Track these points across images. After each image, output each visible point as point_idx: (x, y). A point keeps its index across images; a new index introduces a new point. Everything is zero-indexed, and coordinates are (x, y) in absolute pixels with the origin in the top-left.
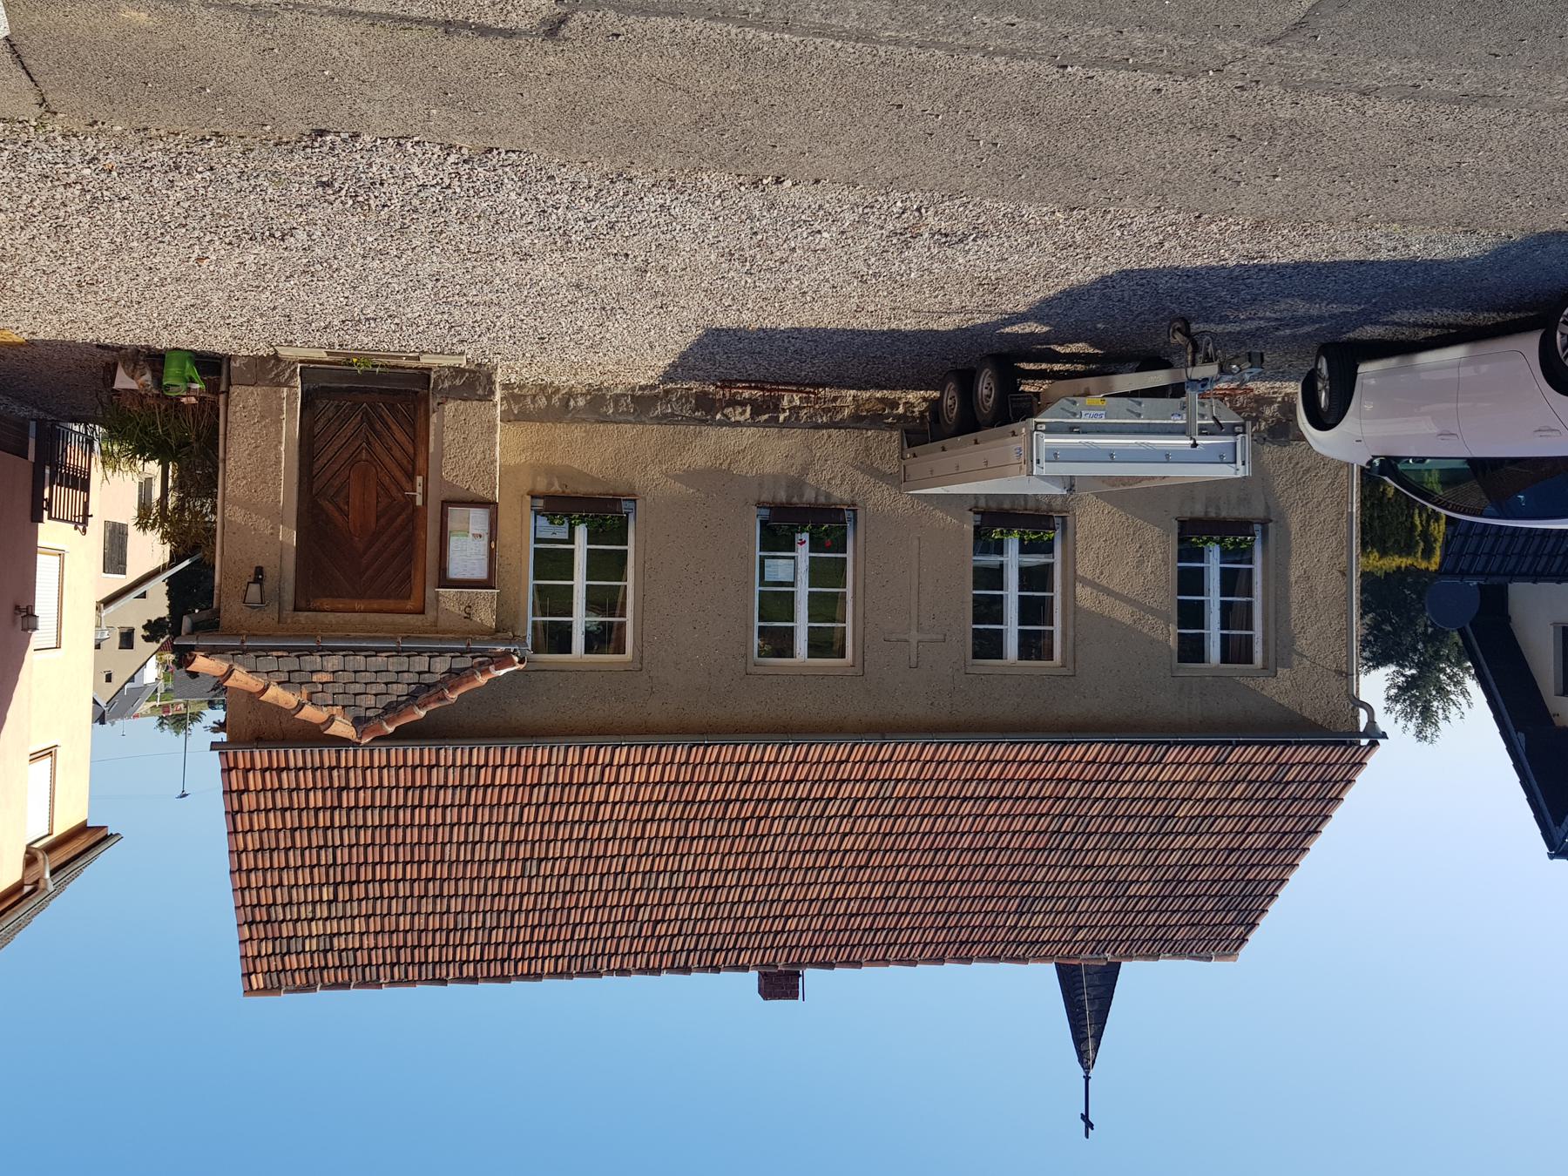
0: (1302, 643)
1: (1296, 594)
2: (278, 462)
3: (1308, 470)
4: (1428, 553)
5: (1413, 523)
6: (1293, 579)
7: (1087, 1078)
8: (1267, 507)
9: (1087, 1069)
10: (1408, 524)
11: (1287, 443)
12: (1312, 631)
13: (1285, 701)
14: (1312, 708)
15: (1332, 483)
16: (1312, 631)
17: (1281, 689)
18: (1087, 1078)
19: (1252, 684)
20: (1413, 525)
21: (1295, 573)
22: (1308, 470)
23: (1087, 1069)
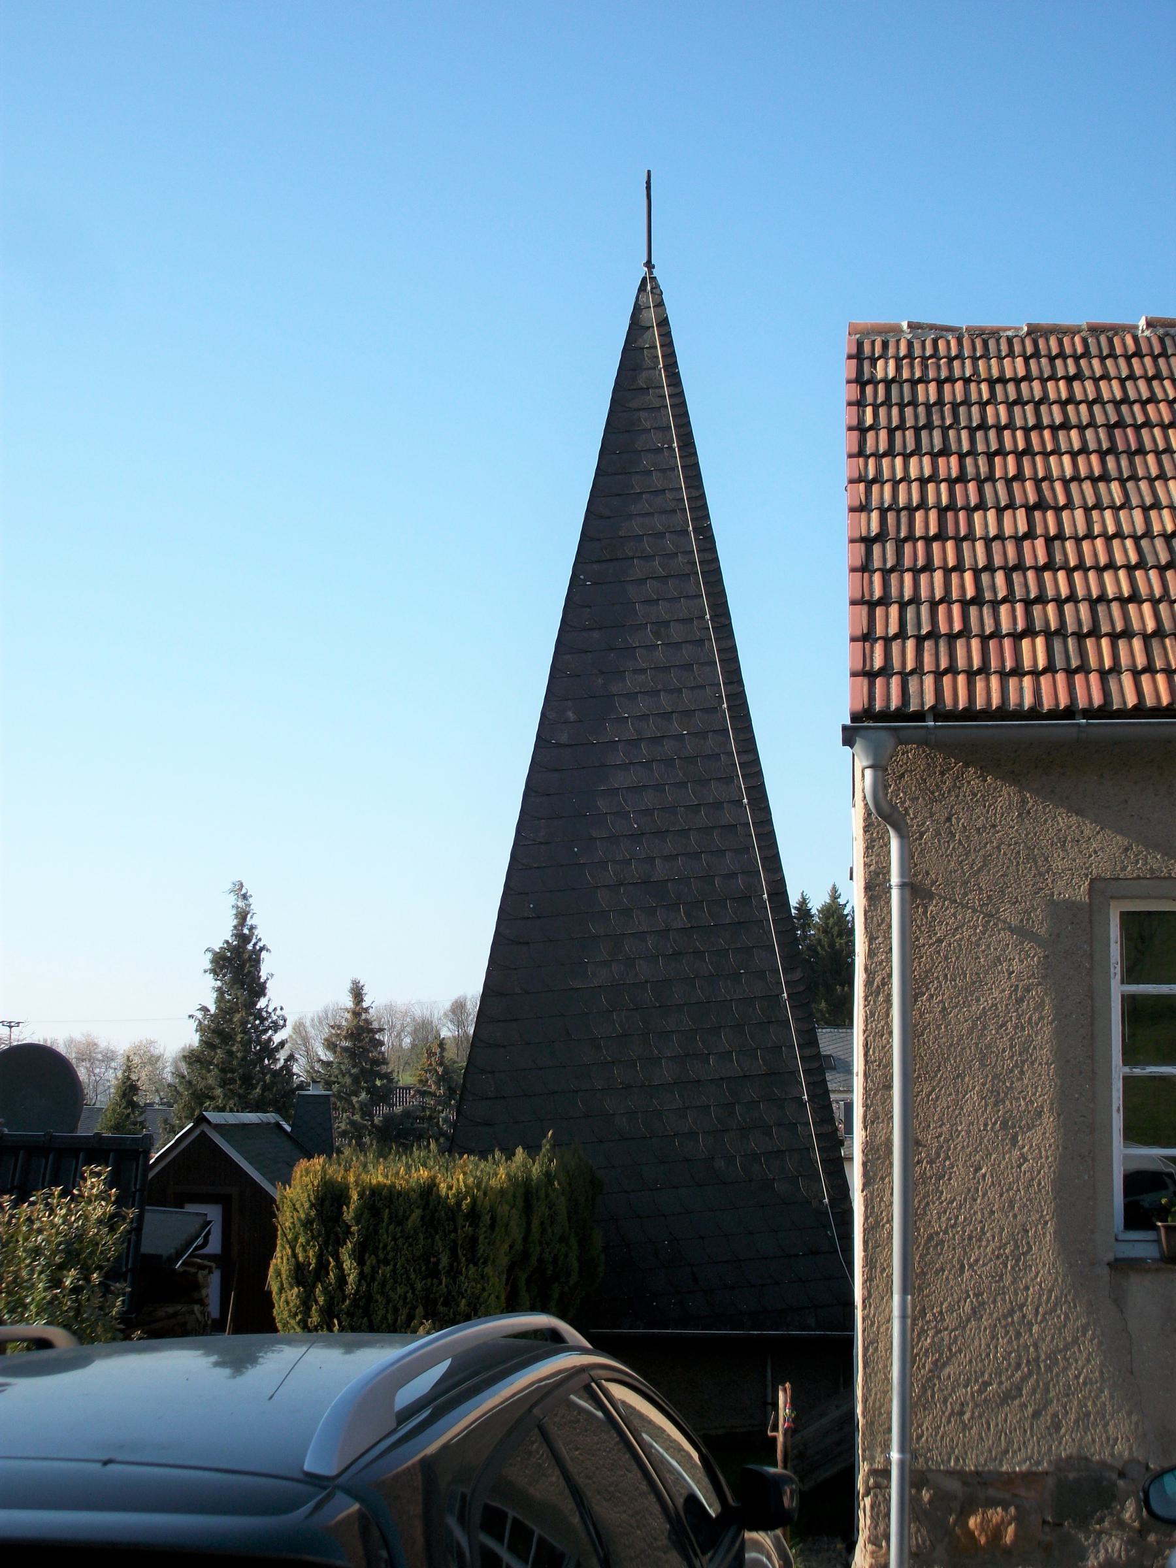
0: (1022, 962)
1: (1039, 1085)
2: (864, 1451)
3: (1006, 1398)
4: (330, 1199)
5: (361, 1262)
6: (1048, 1121)
7: (649, 265)
8: (1119, 1300)
9: (649, 286)
10: (371, 1261)
11: (1062, 1465)
12: (997, 992)
13: (1064, 821)
14: (997, 809)
15: (938, 1366)
16: (997, 992)
17: (1080, 851)
18: (649, 265)
19: (1156, 861)
20: (359, 1256)
21: (1042, 1139)
22: (1006, 1398)
23: (649, 286)
